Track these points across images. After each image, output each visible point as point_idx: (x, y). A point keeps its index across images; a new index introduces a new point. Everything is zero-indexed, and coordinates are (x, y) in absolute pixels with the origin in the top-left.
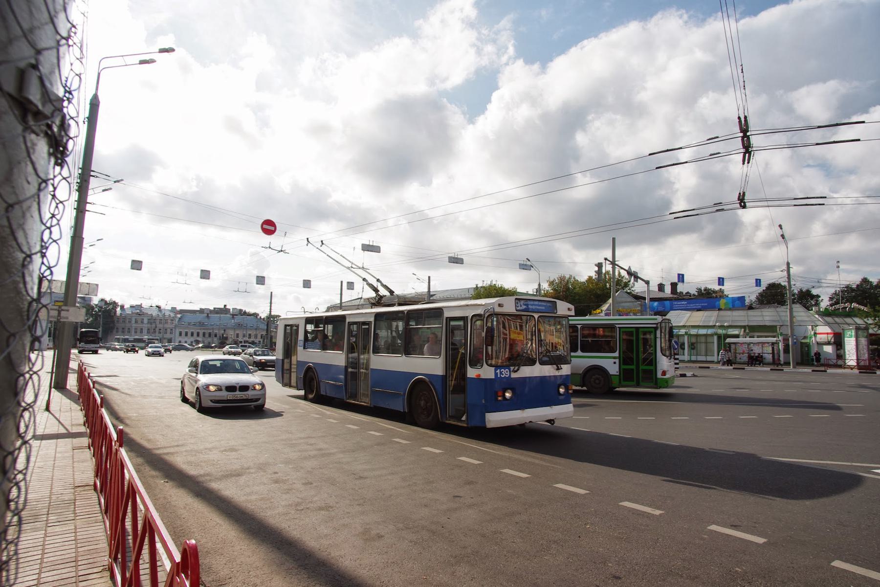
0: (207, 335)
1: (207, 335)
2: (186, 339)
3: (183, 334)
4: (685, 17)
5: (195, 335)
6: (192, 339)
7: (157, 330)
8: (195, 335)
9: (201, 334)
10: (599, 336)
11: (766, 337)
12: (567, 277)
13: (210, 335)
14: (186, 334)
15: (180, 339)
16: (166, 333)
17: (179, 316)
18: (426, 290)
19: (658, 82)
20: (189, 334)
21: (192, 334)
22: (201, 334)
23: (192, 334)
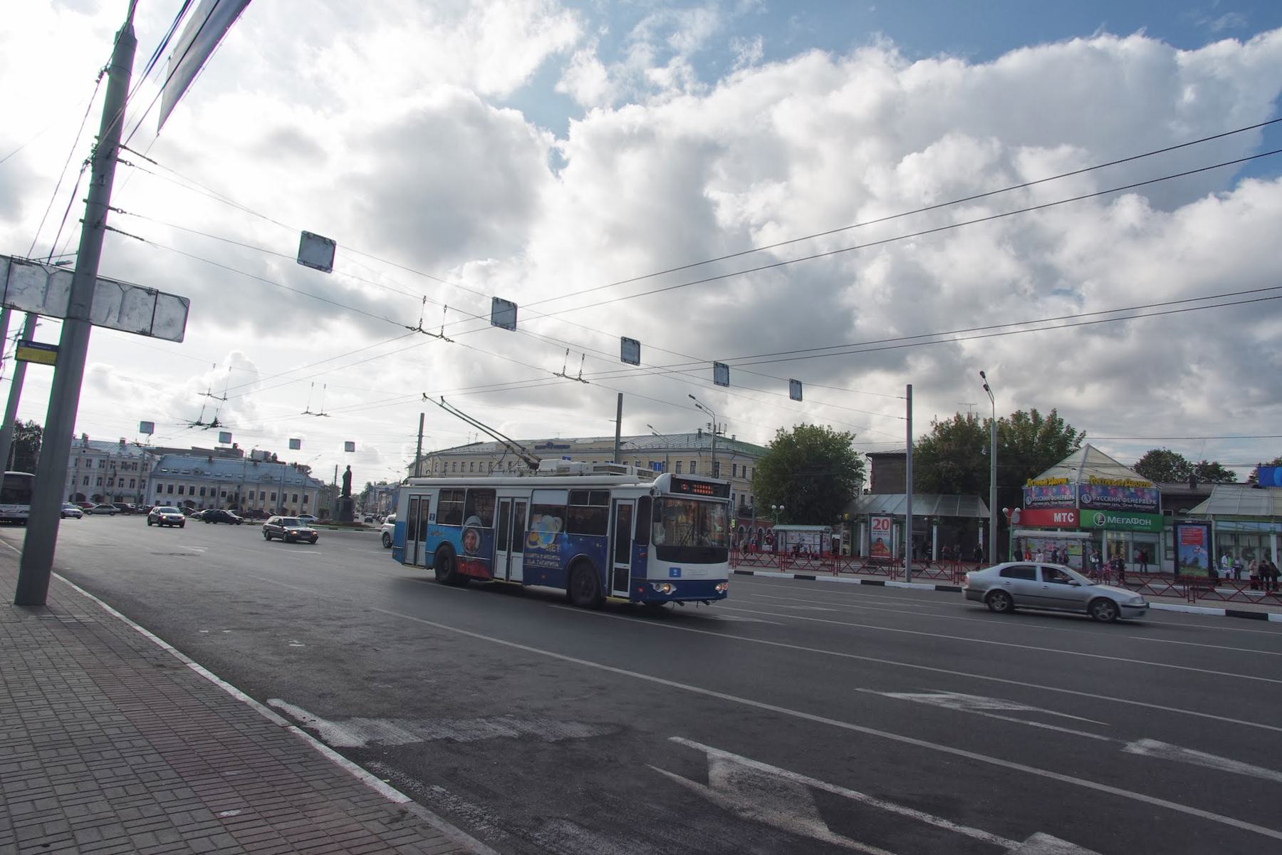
0: (208, 493)
1: (208, 493)
2: (169, 498)
3: (165, 489)
4: (895, 52)
5: (187, 491)
6: (181, 499)
7: (117, 481)
8: (187, 491)
9: (197, 491)
12: (1044, 415)
13: (213, 493)
14: (170, 490)
17: (158, 457)
18: (613, 434)
19: (845, 159)
20: (176, 490)
21: (181, 491)
22: (197, 491)
23: (181, 491)
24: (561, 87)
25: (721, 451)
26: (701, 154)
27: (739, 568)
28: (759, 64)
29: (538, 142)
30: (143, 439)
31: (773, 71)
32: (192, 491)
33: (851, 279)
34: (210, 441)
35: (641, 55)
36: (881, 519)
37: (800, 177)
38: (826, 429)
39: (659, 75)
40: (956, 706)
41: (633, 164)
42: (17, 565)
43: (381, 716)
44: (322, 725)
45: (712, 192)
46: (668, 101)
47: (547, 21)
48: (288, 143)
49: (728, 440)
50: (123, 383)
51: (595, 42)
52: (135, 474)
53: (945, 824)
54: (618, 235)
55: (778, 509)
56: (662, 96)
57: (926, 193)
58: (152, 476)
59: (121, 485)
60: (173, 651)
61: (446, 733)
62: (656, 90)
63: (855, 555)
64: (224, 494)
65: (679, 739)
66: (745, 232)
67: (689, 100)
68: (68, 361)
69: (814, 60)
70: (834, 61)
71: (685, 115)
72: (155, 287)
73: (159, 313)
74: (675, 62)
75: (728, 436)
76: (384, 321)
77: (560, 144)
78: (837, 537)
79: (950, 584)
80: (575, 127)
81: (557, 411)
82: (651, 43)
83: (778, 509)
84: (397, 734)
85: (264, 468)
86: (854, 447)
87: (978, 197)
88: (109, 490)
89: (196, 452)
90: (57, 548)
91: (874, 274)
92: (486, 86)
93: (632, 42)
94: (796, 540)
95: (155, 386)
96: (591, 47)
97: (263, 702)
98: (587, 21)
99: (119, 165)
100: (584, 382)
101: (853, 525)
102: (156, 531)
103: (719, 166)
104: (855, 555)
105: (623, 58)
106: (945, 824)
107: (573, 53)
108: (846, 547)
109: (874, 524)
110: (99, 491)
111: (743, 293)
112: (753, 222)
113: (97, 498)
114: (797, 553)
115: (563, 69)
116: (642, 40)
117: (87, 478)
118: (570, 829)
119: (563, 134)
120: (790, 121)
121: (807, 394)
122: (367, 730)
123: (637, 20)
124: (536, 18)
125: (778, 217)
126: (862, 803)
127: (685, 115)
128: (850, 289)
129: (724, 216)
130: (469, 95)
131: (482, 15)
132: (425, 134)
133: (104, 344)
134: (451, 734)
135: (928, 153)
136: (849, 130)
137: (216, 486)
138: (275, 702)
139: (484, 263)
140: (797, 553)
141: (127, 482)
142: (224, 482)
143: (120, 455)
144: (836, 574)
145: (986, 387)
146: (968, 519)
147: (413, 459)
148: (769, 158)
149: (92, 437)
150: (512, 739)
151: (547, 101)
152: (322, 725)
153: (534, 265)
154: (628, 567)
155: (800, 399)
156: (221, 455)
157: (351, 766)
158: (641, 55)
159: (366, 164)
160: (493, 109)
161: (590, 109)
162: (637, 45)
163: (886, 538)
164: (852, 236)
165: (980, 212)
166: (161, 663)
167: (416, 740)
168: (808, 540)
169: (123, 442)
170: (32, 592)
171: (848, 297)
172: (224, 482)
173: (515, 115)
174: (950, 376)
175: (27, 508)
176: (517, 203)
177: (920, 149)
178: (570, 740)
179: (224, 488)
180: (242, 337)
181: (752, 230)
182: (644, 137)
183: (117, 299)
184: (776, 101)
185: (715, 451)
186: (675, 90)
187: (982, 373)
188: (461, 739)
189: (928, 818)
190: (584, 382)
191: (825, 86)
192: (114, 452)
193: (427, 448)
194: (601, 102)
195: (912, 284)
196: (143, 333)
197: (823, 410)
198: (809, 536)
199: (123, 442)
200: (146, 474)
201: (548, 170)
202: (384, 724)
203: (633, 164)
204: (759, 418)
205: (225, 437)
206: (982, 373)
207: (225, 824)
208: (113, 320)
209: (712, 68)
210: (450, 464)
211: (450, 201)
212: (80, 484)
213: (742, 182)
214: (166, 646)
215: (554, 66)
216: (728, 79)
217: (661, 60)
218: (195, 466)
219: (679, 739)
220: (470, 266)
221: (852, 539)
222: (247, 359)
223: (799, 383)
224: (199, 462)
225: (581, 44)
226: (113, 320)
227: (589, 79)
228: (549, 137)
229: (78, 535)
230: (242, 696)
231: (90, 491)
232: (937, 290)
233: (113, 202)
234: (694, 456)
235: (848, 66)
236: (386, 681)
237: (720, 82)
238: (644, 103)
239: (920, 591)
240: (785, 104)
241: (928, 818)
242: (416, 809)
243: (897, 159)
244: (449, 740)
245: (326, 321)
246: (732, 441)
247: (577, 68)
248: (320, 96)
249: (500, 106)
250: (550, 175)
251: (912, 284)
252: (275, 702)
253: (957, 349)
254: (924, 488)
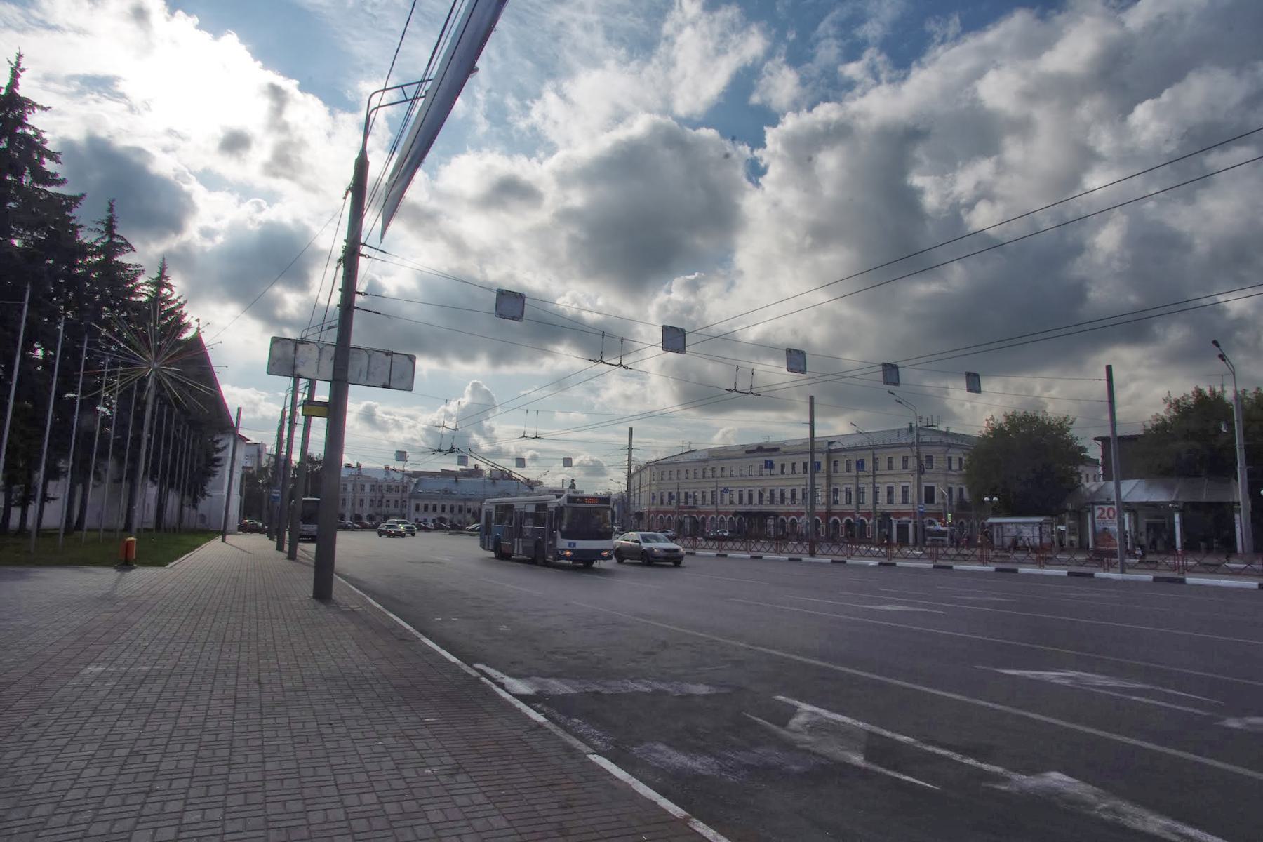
0: (456, 510)
1: (456, 510)
3: (422, 508)
5: (439, 509)
6: (434, 516)
8: (439, 509)
9: (448, 509)
10: (28, 346)
11: (147, 462)
13: (460, 510)
15: (417, 516)
16: (380, 505)
17: (415, 480)
18: (808, 436)
21: (435, 509)
22: (448, 509)
23: (435, 509)
24: (755, 99)
25: (927, 444)
26: (903, 141)
27: (940, 563)
28: (957, 38)
29: (735, 156)
30: (399, 466)
31: (972, 42)
32: (443, 509)
33: (1078, 249)
34: (452, 465)
35: (828, 51)
36: (1106, 507)
37: (1014, 151)
38: (1040, 415)
39: (852, 70)
40: (1066, 682)
41: (829, 162)
42: (313, 570)
43: (550, 676)
44: (508, 680)
45: (917, 180)
46: (864, 94)
47: (734, 38)
48: (508, 192)
49: (939, 432)
50: (387, 417)
51: (783, 48)
52: (398, 496)
53: (971, 761)
54: (821, 235)
55: (991, 501)
56: (858, 91)
57: (1167, 141)
58: (412, 496)
59: (388, 506)
60: (412, 630)
61: (596, 688)
62: (850, 85)
63: (1083, 547)
64: (469, 510)
65: (782, 698)
66: (956, 213)
67: (885, 89)
68: (334, 412)
69: (1018, 21)
70: (1042, 17)
71: (881, 104)
72: (390, 349)
73: (396, 374)
74: (869, 54)
75: (942, 428)
76: (605, 343)
77: (757, 153)
78: (1063, 528)
79: (1174, 575)
80: (771, 134)
81: (772, 415)
82: (836, 37)
83: (991, 501)
84: (559, 687)
86: (1073, 432)
87: (1241, 137)
88: (379, 510)
89: (445, 473)
90: (337, 559)
91: (1108, 239)
92: (683, 106)
93: (818, 40)
94: (1014, 532)
95: (411, 417)
96: (780, 55)
97: (471, 666)
98: (774, 31)
99: (361, 259)
100: (756, 395)
101: (1079, 516)
102: (384, 539)
103: (919, 152)
104: (1083, 547)
105: (811, 59)
106: (971, 761)
107: (762, 65)
108: (1073, 538)
109: (1098, 513)
110: (371, 512)
111: (958, 277)
112: (963, 201)
113: (371, 518)
114: (1015, 546)
115: (755, 82)
116: (827, 37)
117: (362, 500)
118: (661, 747)
119: (759, 142)
120: (998, 91)
121: (986, 385)
122: (540, 684)
123: (820, 19)
124: (723, 36)
125: (986, 195)
126: (1075, 801)
127: (881, 104)
128: (1079, 261)
129: (931, 201)
130: (668, 121)
131: (673, 43)
132: (626, 163)
133: (358, 400)
134: (599, 689)
135: (1166, 96)
136: (1065, 90)
137: (462, 504)
138: (478, 666)
139: (692, 277)
140: (1015, 546)
141: (392, 504)
142: (469, 500)
143: (386, 480)
144: (1042, 567)
146: (1220, 504)
148: (979, 133)
149: (365, 465)
150: (645, 693)
151: (741, 114)
152: (508, 680)
153: (741, 273)
155: (978, 391)
156: (466, 476)
157: (520, 705)
158: (828, 51)
159: (577, 199)
160: (690, 130)
161: (784, 115)
162: (823, 43)
163: (1114, 528)
164: (1078, 205)
165: (1242, 153)
166: (404, 638)
167: (571, 691)
168: (1027, 532)
169: (387, 468)
170: (322, 591)
171: (1077, 269)
172: (469, 500)
173: (708, 133)
174: (1216, 344)
175: (315, 527)
176: (720, 217)
177: (1155, 93)
178: (691, 696)
179: (470, 505)
180: (472, 372)
181: (962, 212)
182: (838, 133)
183: (365, 362)
184: (979, 73)
185: (920, 444)
186: (870, 81)
188: (606, 692)
189: (957, 757)
190: (756, 395)
191: (1034, 47)
192: (381, 477)
193: (640, 458)
194: (796, 107)
195: (1154, 245)
196: (384, 386)
197: (1058, 393)
198: (1028, 527)
199: (387, 468)
200: (406, 495)
201: (745, 180)
202: (553, 681)
203: (829, 162)
204: (977, 411)
205: (463, 460)
207: (427, 725)
208: (363, 379)
209: (904, 51)
210: (667, 473)
211: (654, 220)
212: (357, 506)
213: (947, 164)
214: (407, 626)
215: (745, 80)
216: (923, 60)
217: (853, 52)
218: (443, 487)
219: (782, 698)
220: (678, 282)
221: (1080, 530)
222: (485, 387)
223: (976, 376)
224: (446, 483)
225: (770, 54)
226: (363, 379)
227: (783, 85)
228: (745, 150)
229: (353, 547)
230: (453, 659)
231: (366, 511)
232: (1187, 247)
234: (907, 452)
235: (1059, 19)
236: (564, 654)
237: (914, 63)
238: (839, 100)
239: (1137, 583)
240: (992, 77)
241: (957, 757)
242: (551, 727)
243: (1130, 110)
244: (597, 693)
245: (550, 347)
246: (946, 434)
247: (768, 77)
248: (534, 144)
249: (696, 126)
250: (749, 185)
251: (1154, 245)
252: (478, 666)
253: (1217, 309)
254: (1160, 473)
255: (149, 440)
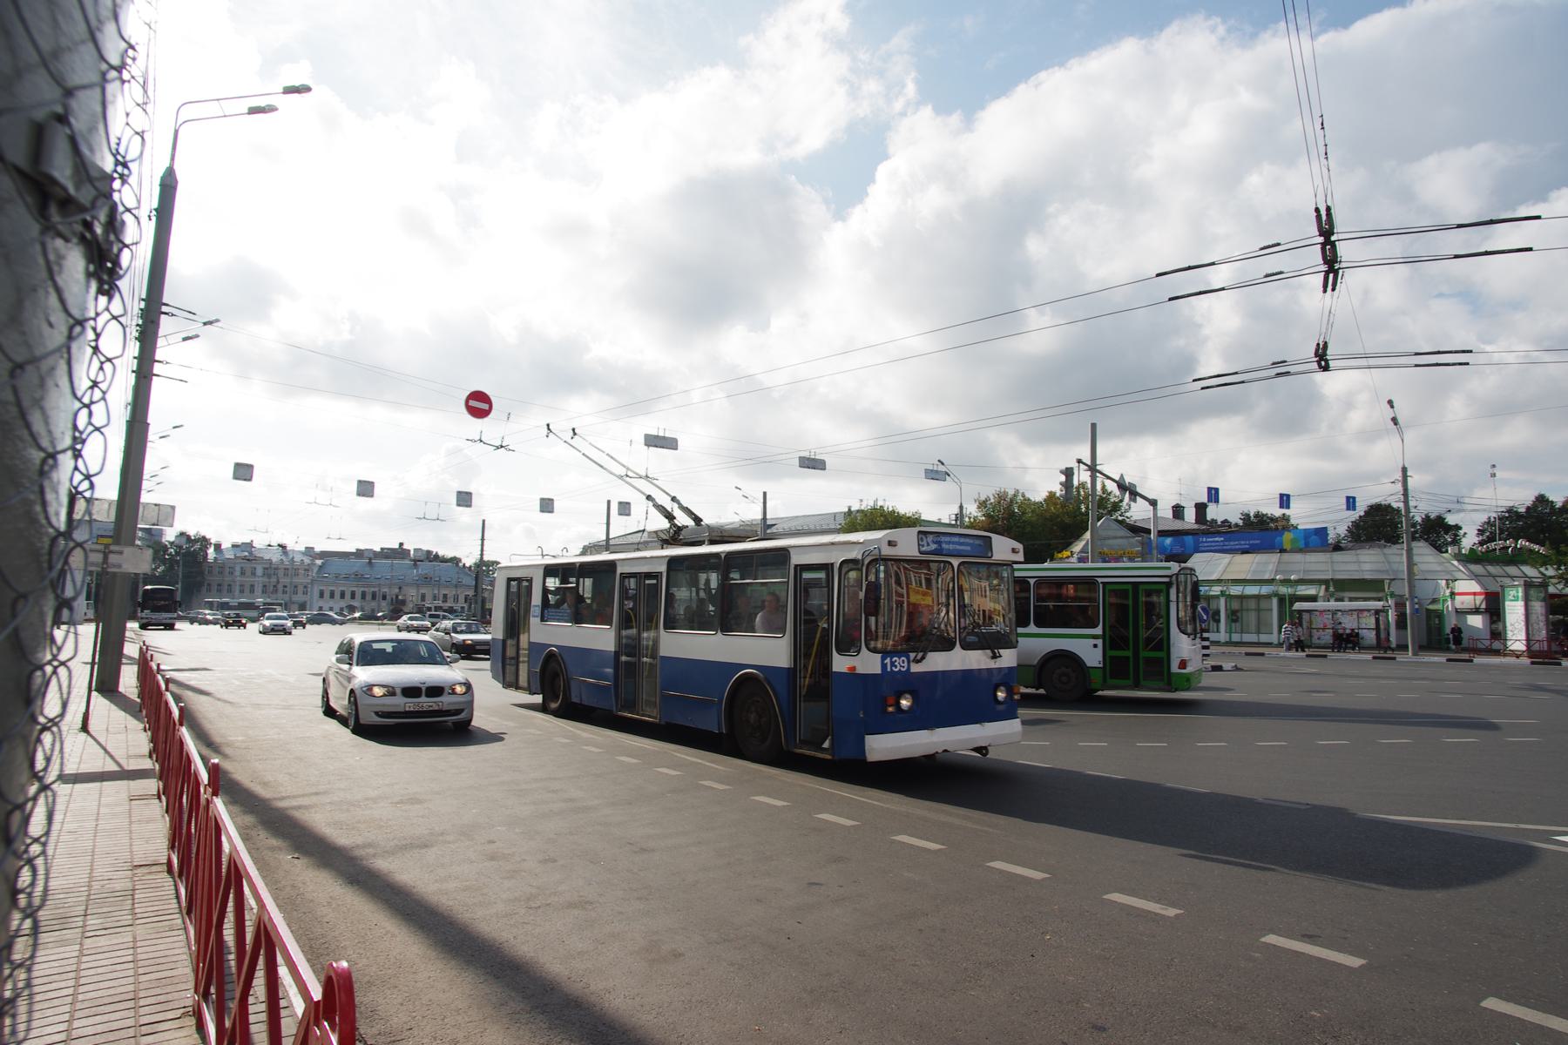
0: (369, 597)
1: (369, 597)
2: (331, 603)
3: (327, 594)
4: (1221, 30)
5: (348, 595)
6: (343, 604)
7: (280, 587)
8: (348, 595)
9: (358, 595)
13: (374, 596)
14: (332, 595)
15: (321, 603)
16: (296, 593)
17: (319, 562)
18: (760, 517)
20: (337, 595)
21: (343, 595)
22: (358, 595)
32: (353, 596)
40: (51, 707)
85: (425, 568)
145: (1395, 421)
147: (1139, 490)
151: (850, 165)
154: (1129, 653)
176: (787, 256)
187: (1390, 402)
206: (1390, 402)
233: (159, 355)
255: (1351, 599)
